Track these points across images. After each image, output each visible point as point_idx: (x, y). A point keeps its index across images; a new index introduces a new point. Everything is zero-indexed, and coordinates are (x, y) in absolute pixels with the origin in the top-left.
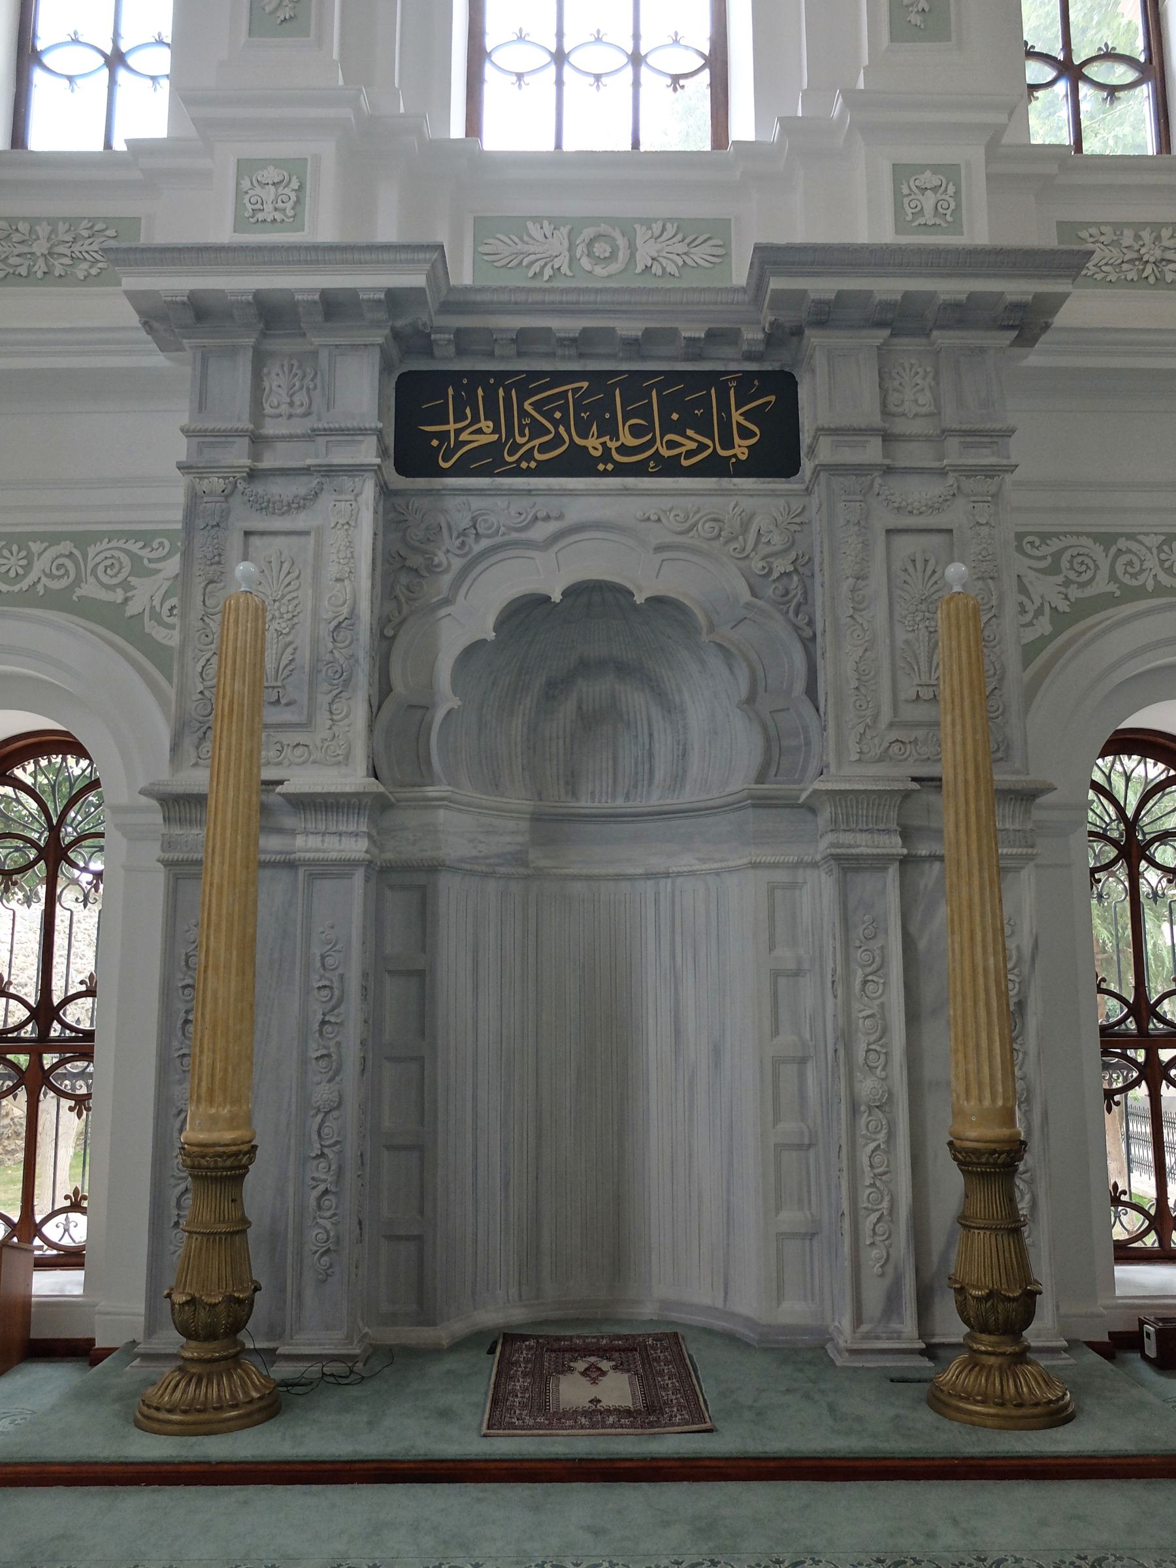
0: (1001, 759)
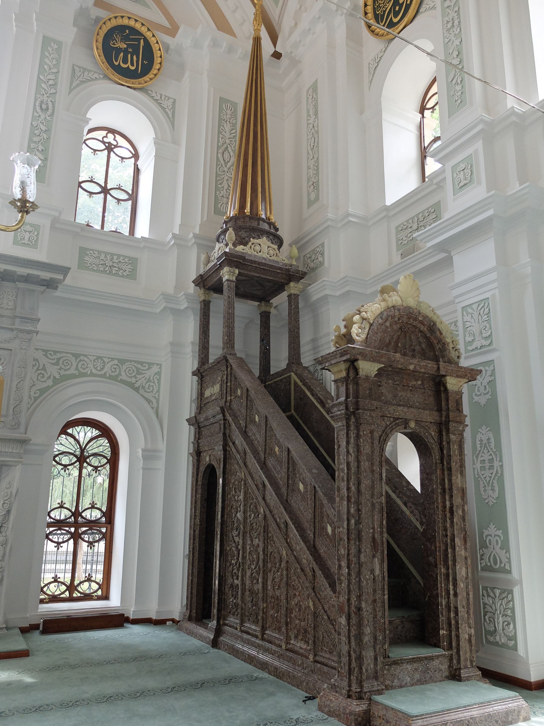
0: (16, 428)
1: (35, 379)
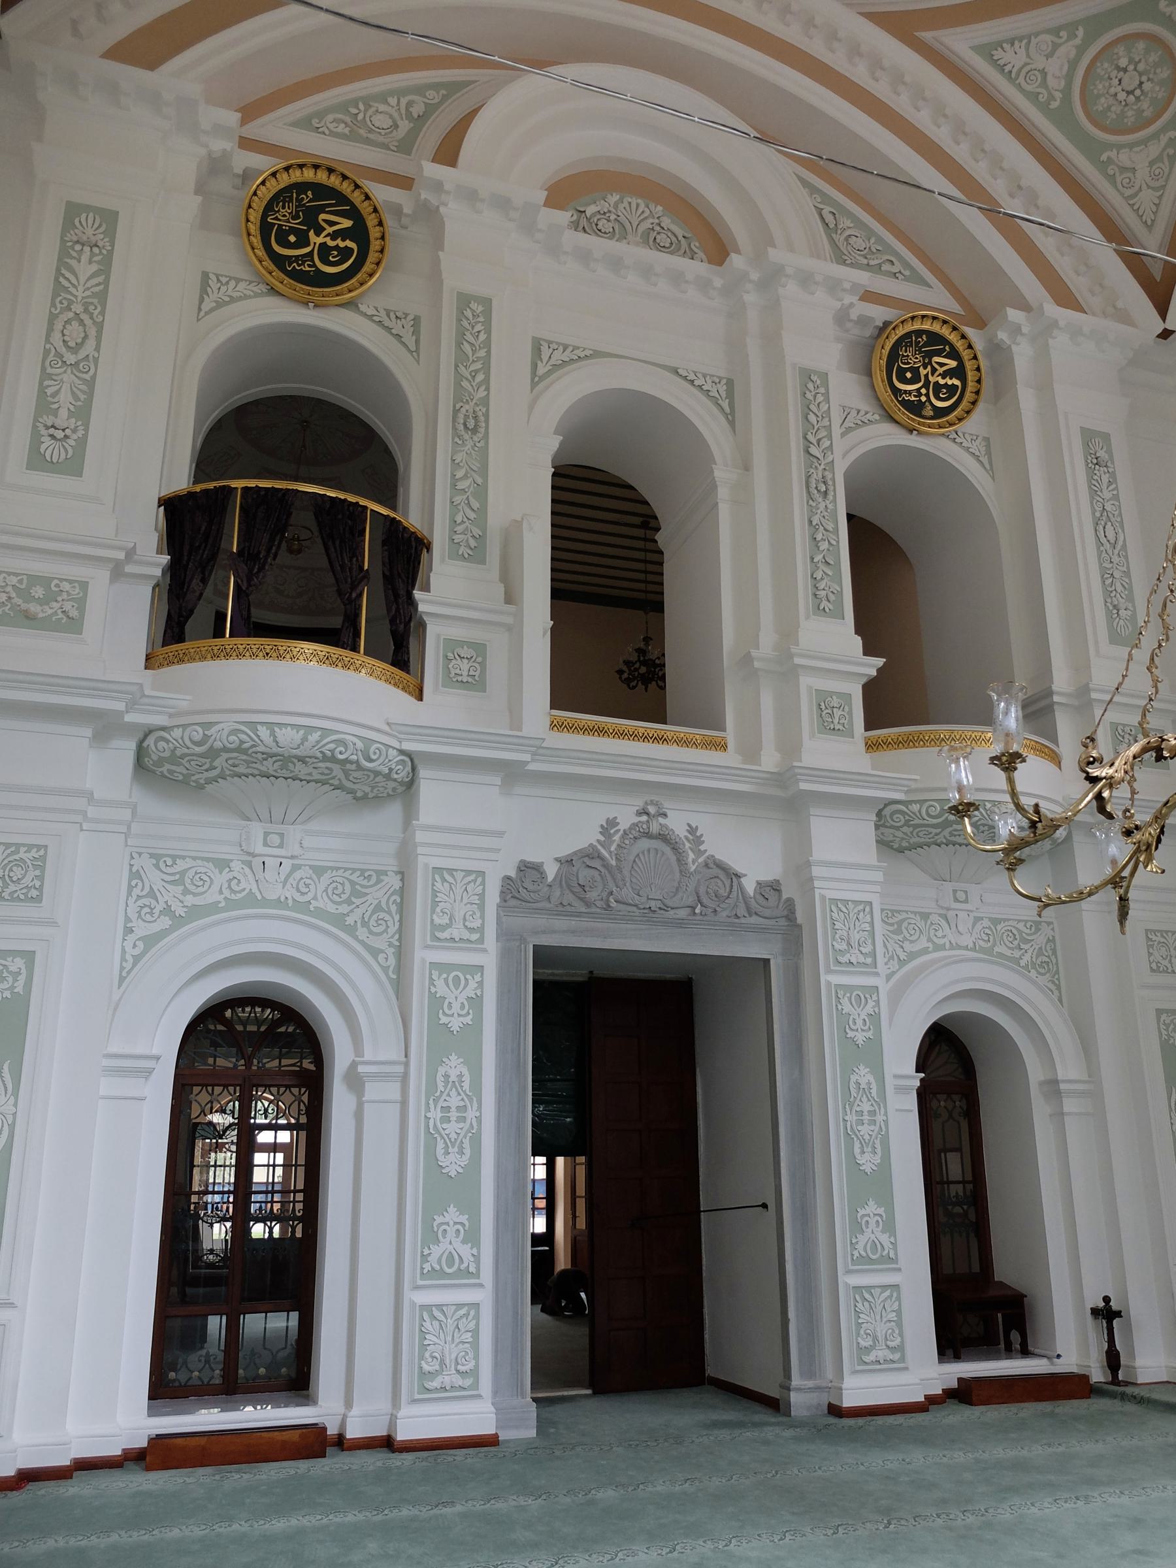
1: (133, 915)
